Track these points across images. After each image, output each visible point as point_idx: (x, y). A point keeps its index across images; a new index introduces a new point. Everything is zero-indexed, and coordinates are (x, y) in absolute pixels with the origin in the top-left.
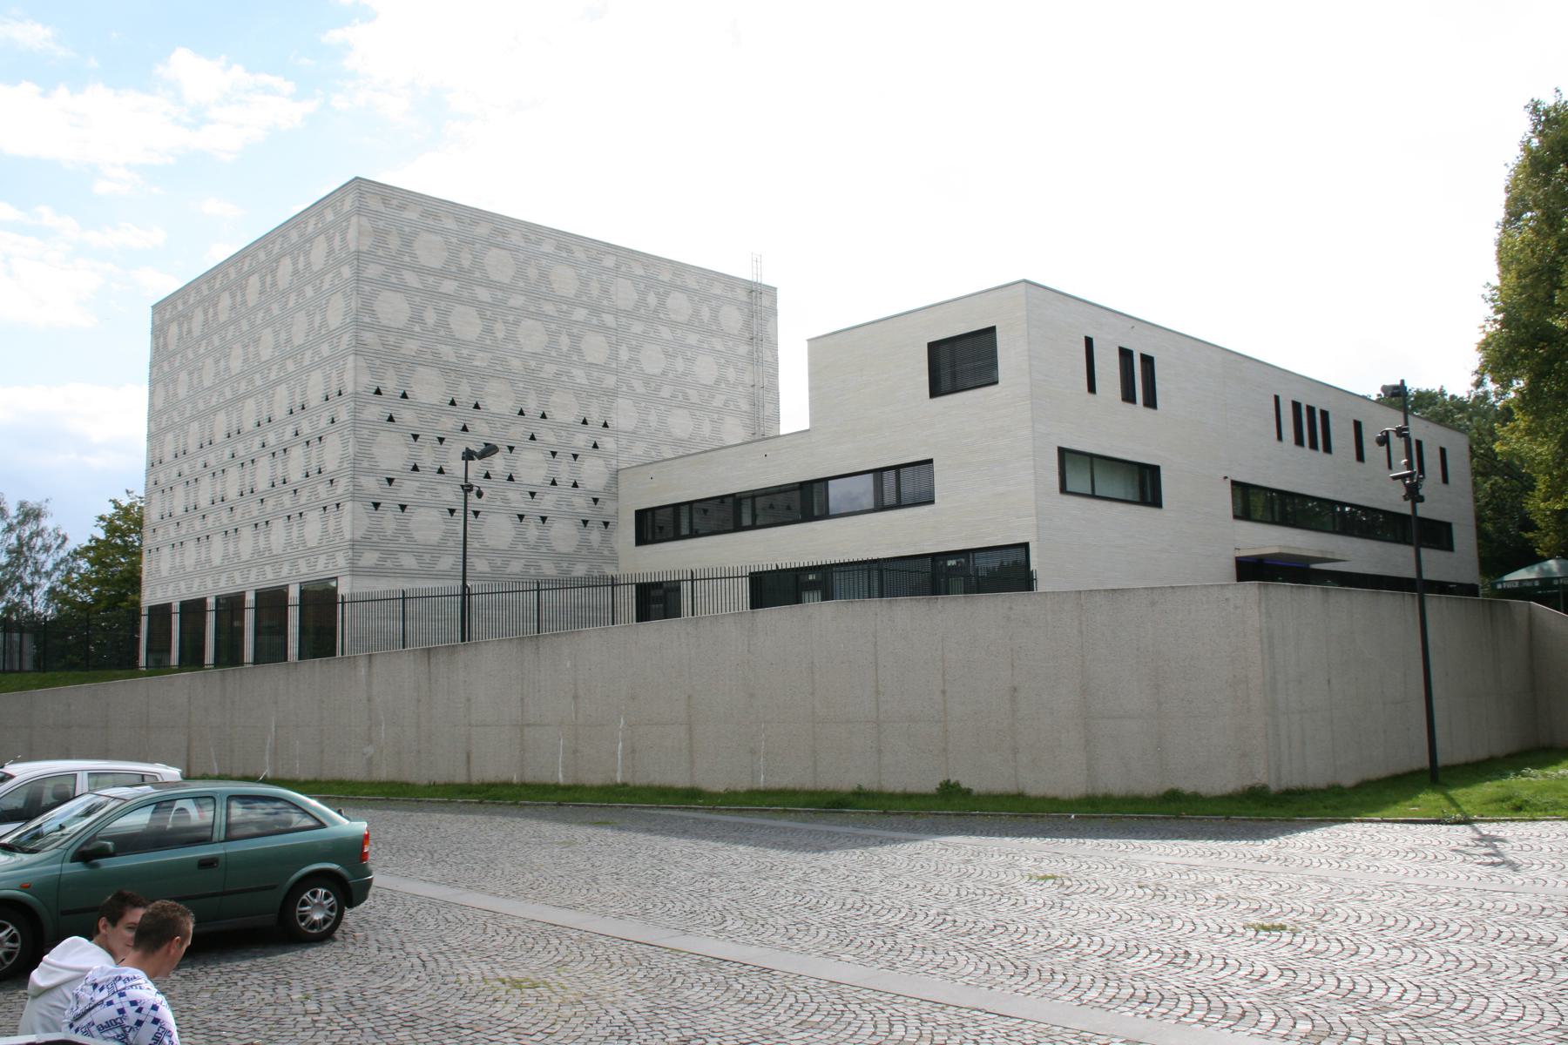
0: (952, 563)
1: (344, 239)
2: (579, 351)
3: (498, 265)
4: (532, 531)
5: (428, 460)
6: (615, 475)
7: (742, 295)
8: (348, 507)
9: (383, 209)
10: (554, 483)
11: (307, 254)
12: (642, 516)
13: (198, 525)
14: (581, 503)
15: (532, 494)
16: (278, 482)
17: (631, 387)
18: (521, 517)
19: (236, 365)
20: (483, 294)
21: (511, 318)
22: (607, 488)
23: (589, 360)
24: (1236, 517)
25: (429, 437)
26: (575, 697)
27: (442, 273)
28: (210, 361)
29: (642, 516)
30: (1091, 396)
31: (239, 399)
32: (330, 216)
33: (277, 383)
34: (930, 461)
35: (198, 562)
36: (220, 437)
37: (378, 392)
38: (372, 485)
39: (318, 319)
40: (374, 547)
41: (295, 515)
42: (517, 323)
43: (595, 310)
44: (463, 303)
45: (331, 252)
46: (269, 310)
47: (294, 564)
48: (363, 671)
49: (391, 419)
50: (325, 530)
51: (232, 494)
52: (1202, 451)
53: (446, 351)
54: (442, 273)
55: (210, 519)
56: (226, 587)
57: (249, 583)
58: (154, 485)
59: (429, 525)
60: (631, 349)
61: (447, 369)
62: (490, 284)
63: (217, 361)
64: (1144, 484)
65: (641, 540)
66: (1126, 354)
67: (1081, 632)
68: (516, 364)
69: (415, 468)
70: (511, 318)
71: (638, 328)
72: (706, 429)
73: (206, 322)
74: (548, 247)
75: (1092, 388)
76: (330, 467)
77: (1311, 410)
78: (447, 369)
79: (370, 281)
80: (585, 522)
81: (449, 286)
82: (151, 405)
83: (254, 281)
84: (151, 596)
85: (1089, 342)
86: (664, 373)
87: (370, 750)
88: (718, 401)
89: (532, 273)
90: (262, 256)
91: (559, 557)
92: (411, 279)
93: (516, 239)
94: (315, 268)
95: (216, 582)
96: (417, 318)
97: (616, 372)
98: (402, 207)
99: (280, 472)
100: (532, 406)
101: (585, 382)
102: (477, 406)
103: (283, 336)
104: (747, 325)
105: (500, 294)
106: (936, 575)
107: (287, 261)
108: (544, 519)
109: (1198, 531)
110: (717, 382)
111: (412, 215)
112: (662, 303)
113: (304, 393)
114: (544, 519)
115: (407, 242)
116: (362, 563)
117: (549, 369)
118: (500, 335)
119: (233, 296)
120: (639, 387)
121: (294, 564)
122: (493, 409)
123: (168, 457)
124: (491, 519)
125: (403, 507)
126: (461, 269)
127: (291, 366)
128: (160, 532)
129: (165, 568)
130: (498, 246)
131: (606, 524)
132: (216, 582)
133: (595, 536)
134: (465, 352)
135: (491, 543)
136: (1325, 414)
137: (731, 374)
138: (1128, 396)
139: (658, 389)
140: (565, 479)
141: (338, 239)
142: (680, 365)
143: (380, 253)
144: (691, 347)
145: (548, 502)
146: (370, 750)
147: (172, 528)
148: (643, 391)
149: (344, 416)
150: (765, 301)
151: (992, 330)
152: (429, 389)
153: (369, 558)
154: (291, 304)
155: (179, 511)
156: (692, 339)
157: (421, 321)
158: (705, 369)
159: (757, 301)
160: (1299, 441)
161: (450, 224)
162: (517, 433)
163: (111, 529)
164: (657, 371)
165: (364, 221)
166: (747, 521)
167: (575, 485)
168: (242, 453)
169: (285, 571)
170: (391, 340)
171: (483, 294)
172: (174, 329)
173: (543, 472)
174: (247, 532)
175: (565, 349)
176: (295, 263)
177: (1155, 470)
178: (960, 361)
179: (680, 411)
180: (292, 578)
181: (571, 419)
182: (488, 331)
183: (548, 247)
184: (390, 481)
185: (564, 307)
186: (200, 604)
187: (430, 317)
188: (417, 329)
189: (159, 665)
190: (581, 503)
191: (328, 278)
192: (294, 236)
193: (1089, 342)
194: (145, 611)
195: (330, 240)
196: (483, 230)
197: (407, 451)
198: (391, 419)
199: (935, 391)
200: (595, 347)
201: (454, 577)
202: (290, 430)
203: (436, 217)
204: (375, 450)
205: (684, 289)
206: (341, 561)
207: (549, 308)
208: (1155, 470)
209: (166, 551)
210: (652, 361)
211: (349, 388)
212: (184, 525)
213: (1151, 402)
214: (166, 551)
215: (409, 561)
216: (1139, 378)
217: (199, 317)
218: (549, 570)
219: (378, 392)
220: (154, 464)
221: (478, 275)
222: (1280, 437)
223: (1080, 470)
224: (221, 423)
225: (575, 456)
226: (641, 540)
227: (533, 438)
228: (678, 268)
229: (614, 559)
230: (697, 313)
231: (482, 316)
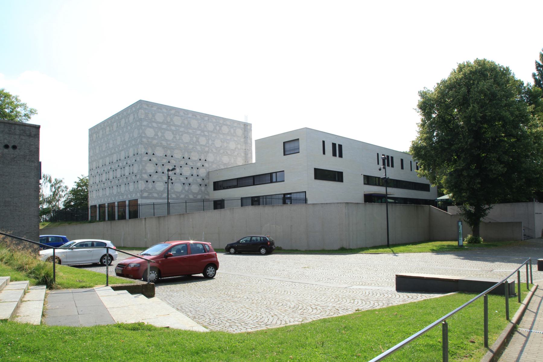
0: (289, 196)
2: (198, 142)
3: (177, 121)
4: (187, 187)
5: (160, 170)
6: (208, 173)
7: (243, 126)
8: (140, 182)
9: (147, 107)
11: (128, 118)
12: (215, 183)
13: (102, 185)
14: (199, 180)
17: (212, 151)
19: (111, 146)
20: (173, 128)
22: (206, 176)
24: (365, 184)
25: (160, 164)
28: (104, 144)
29: (215, 183)
31: (112, 154)
32: (134, 109)
33: (122, 150)
35: (103, 195)
36: (107, 163)
37: (147, 153)
38: (145, 176)
39: (131, 135)
40: (147, 192)
41: (127, 183)
42: (182, 135)
43: (203, 131)
44: (168, 130)
45: (134, 118)
47: (127, 196)
48: (144, 222)
49: (150, 160)
50: (134, 188)
51: (111, 178)
52: (353, 169)
53: (164, 143)
54: (163, 123)
55: (106, 184)
56: (110, 201)
57: (116, 200)
58: (90, 175)
59: (160, 186)
60: (212, 141)
61: (164, 147)
62: (175, 125)
64: (337, 177)
65: (215, 189)
68: (182, 145)
69: (157, 172)
71: (214, 135)
72: (232, 161)
73: (103, 134)
74: (190, 115)
75: (324, 153)
76: (135, 172)
78: (164, 147)
79: (144, 126)
81: (164, 126)
83: (115, 124)
84: (91, 203)
85: (324, 142)
86: (221, 147)
88: (236, 153)
89: (186, 122)
90: (117, 118)
91: (194, 194)
92: (155, 125)
96: (156, 135)
98: (152, 107)
99: (123, 173)
100: (186, 156)
103: (123, 139)
106: (286, 199)
107: (123, 120)
109: (353, 189)
111: (155, 108)
112: (220, 129)
115: (154, 116)
117: (191, 147)
118: (178, 138)
119: (110, 128)
120: (214, 150)
121: (127, 196)
123: (94, 168)
125: (154, 182)
127: (125, 146)
128: (93, 187)
129: (94, 196)
130: (177, 116)
132: (108, 200)
133: (203, 188)
134: (169, 143)
135: (176, 190)
137: (239, 146)
138: (334, 154)
140: (195, 174)
141: (136, 115)
142: (225, 145)
144: (228, 140)
145: (191, 180)
147: (96, 186)
149: (138, 159)
150: (249, 127)
152: (160, 152)
153: (145, 194)
154: (125, 130)
155: (97, 182)
156: (229, 138)
157: (157, 135)
158: (232, 145)
159: (246, 127)
161: (164, 110)
162: (182, 163)
163: (79, 185)
164: (219, 146)
169: (125, 197)
170: (150, 140)
171: (173, 128)
172: (95, 135)
174: (115, 187)
176: (125, 120)
180: (127, 198)
182: (175, 137)
183: (190, 115)
184: (150, 175)
186: (95, 206)
187: (160, 134)
189: (93, 221)
190: (199, 180)
192: (125, 113)
193: (324, 142)
194: (89, 207)
195: (134, 115)
196: (173, 112)
198: (150, 160)
200: (203, 141)
201: (164, 198)
202: (125, 163)
203: (161, 109)
204: (146, 168)
205: (226, 125)
206: (138, 195)
207: (190, 131)
209: (95, 192)
210: (218, 143)
211: (140, 153)
212: (99, 186)
213: (341, 156)
214: (95, 192)
215: (155, 195)
216: (338, 150)
217: (101, 133)
218: (191, 197)
219: (147, 153)
222: (378, 164)
223: (321, 174)
224: (108, 160)
226: (215, 189)
228: (225, 120)
229: (208, 194)
231: (173, 134)
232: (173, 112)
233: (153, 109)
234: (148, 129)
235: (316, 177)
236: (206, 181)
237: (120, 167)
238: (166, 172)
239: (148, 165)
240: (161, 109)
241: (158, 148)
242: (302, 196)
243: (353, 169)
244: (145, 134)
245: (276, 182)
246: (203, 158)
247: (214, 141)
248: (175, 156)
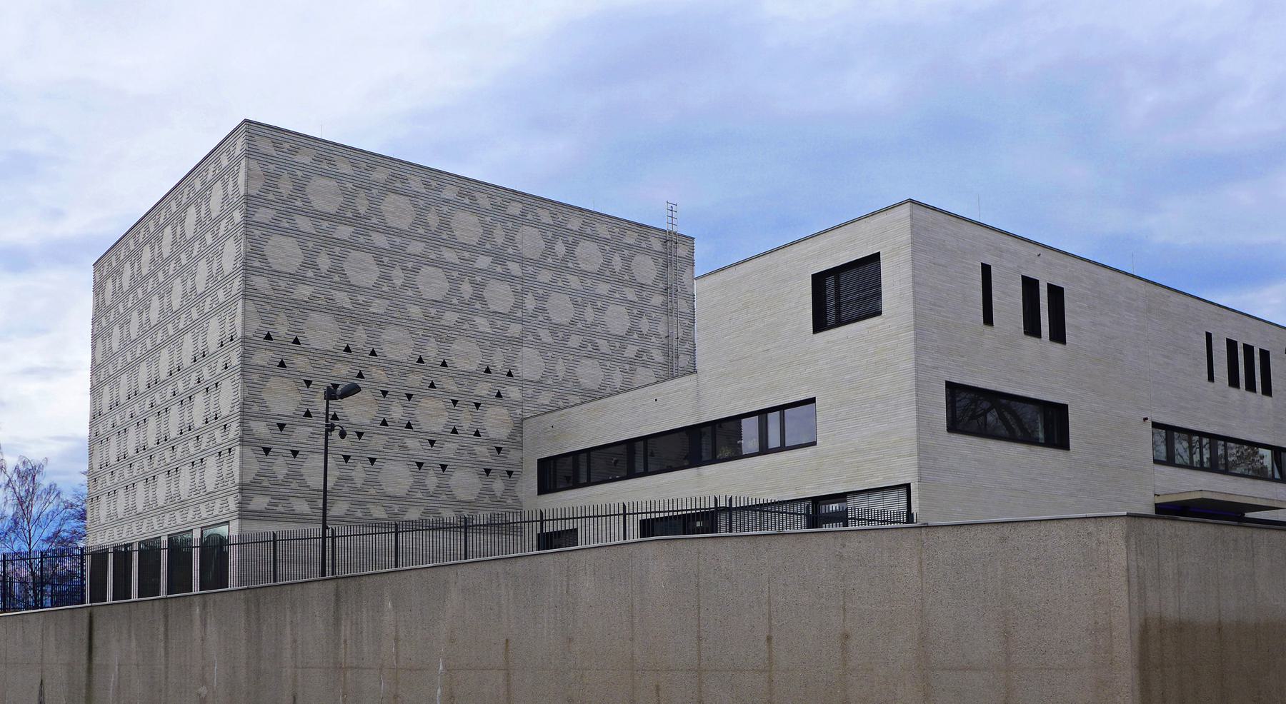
1: (235, 184)
2: (482, 299)
6: (519, 425)
7: (657, 245)
10: (454, 431)
15: (432, 442)
16: (185, 430)
17: (537, 337)
18: (420, 465)
21: (410, 265)
22: (511, 436)
23: (493, 308)
26: (397, 640)
27: (337, 218)
28: (135, 314)
30: (988, 328)
34: (812, 401)
39: (215, 265)
40: (264, 491)
42: (415, 270)
43: (499, 258)
46: (179, 260)
49: (282, 364)
52: (1114, 387)
53: (342, 298)
54: (337, 218)
57: (160, 528)
60: (538, 298)
62: (388, 230)
63: (141, 313)
64: (1047, 424)
65: (544, 489)
66: (1030, 286)
67: (921, 572)
68: (415, 311)
70: (410, 265)
71: (545, 276)
74: (449, 193)
77: (1249, 350)
78: (340, 314)
79: (260, 224)
80: (488, 471)
81: (344, 232)
82: (93, 360)
86: (573, 323)
87: (203, 690)
89: (433, 220)
92: (304, 224)
93: (416, 184)
94: (214, 215)
95: (140, 528)
96: (309, 263)
97: (521, 321)
101: (489, 330)
102: (373, 353)
104: (662, 276)
105: (398, 240)
106: (820, 512)
108: (444, 467)
109: (1113, 469)
110: (629, 332)
111: (304, 158)
112: (570, 252)
113: (205, 341)
114: (444, 467)
115: (300, 188)
116: (252, 506)
118: (398, 282)
122: (390, 356)
124: (388, 466)
125: (295, 453)
126: (357, 215)
129: (103, 513)
131: (510, 473)
132: (140, 528)
133: (498, 486)
134: (361, 299)
135: (390, 490)
136: (1265, 355)
137: (644, 325)
138: (1032, 328)
139: (566, 339)
140: (466, 424)
141: (231, 183)
143: (271, 197)
145: (449, 448)
146: (203, 690)
148: (550, 340)
150: (682, 251)
151: (876, 257)
152: (322, 333)
153: (260, 502)
156: (603, 288)
157: (315, 266)
160: (1234, 382)
164: (565, 320)
165: (254, 165)
166: (639, 467)
167: (477, 434)
168: (158, 402)
171: (380, 240)
172: (109, 285)
173: (443, 421)
175: (467, 297)
176: (198, 212)
177: (1063, 409)
178: (843, 294)
179: (589, 362)
181: (474, 368)
182: (386, 278)
185: (467, 255)
187: (324, 262)
188: (310, 274)
191: (223, 223)
197: (299, 397)
198: (282, 364)
199: (820, 325)
203: (331, 162)
204: (265, 395)
208: (1063, 409)
209: (104, 499)
213: (1058, 335)
216: (1045, 310)
219: (268, 337)
220: (96, 416)
221: (374, 220)
222: (1211, 378)
225: (478, 405)
226: (544, 489)
227: (432, 386)
230: (608, 262)
231: (379, 262)
232: (380, 175)
233: (298, 158)
234: (276, 239)
235: (955, 426)
236: (514, 456)
237: (178, 399)
238: (319, 405)
239: (274, 383)
240: (331, 162)
241: (315, 316)
242: (894, 504)
243: (1114, 387)
244: (263, 258)
245: (783, 448)
246: (499, 365)
247: (543, 298)
248: (388, 352)
